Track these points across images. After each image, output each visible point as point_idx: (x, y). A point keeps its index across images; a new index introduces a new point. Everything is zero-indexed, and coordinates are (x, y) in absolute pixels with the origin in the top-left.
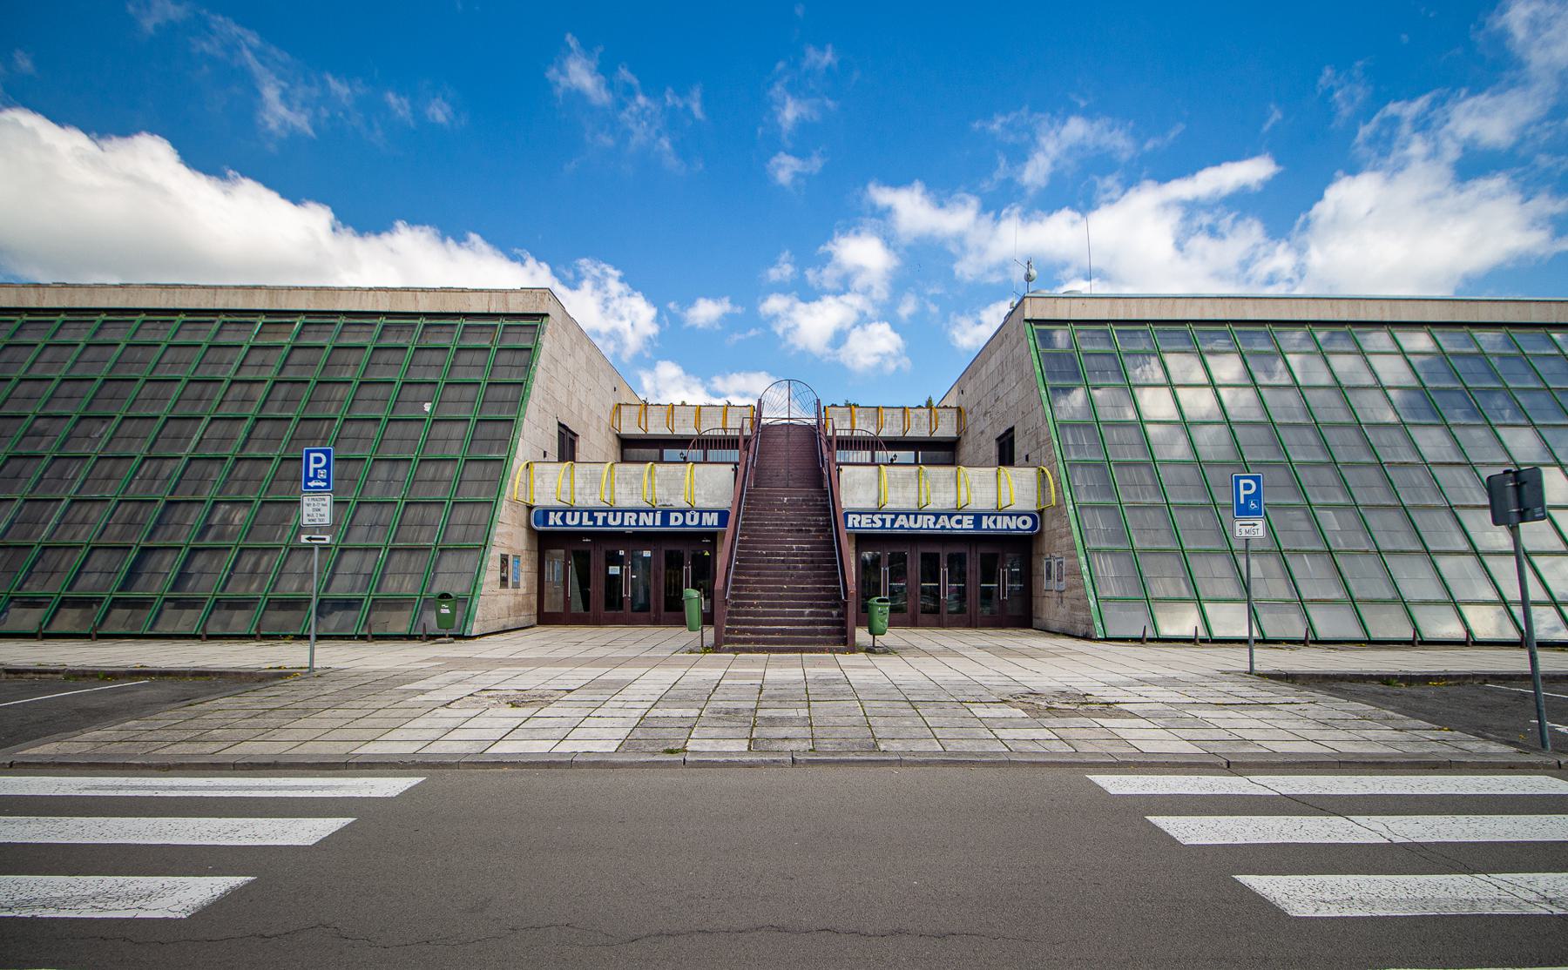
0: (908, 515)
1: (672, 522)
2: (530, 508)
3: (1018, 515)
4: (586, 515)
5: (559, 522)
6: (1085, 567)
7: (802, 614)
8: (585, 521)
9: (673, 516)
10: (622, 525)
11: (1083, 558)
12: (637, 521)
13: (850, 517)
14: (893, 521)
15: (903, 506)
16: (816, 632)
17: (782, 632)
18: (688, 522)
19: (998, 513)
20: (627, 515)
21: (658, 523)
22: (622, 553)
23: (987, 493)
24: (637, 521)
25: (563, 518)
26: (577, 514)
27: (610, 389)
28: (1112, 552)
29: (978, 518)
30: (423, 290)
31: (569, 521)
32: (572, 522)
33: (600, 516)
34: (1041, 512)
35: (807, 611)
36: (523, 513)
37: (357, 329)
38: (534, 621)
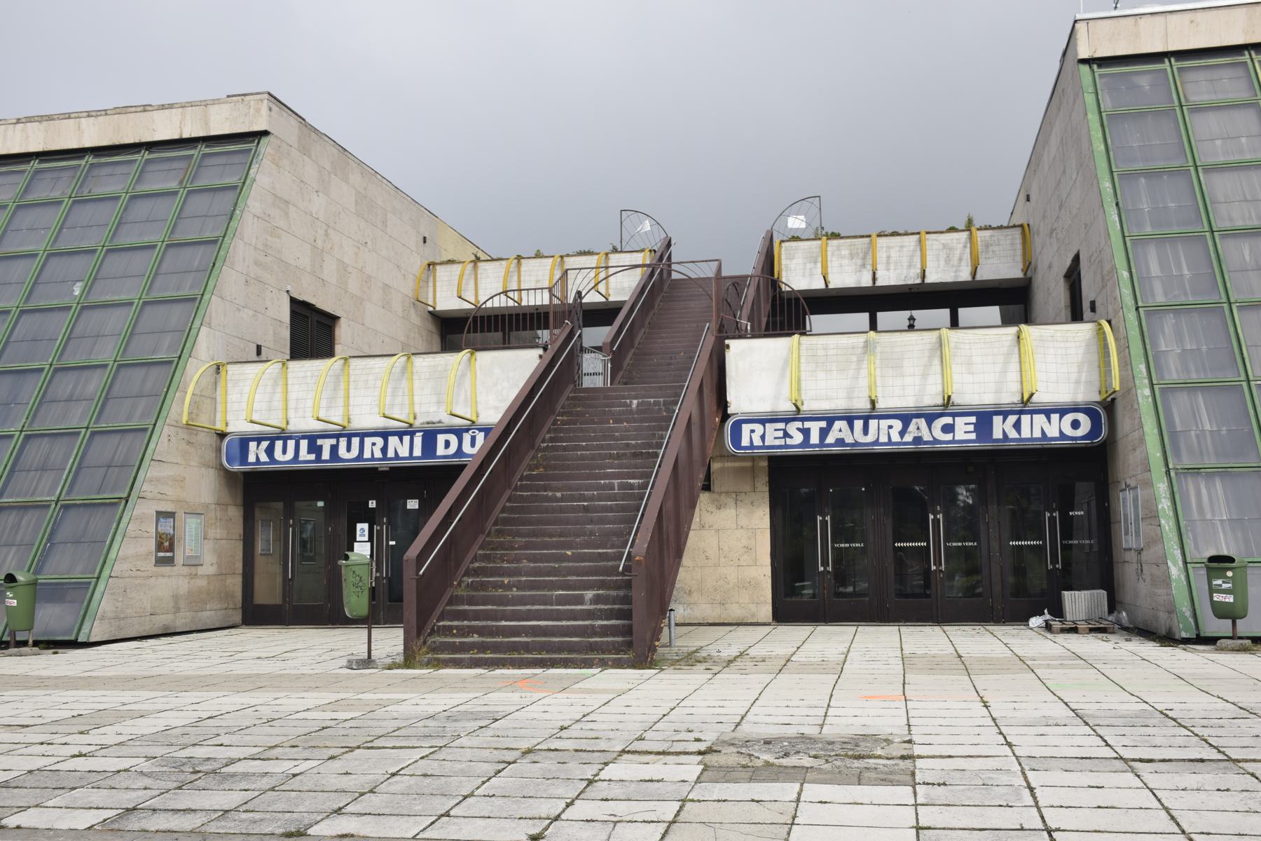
0: (850, 420)
1: (441, 450)
2: (222, 435)
3: (1063, 411)
4: (304, 444)
5: (264, 458)
6: (1165, 504)
9: (441, 439)
11: (1162, 487)
12: (384, 450)
13: (746, 428)
14: (824, 433)
15: (837, 403)
18: (467, 448)
19: (1025, 407)
21: (417, 452)
22: (372, 504)
23: (1032, 376)
24: (384, 450)
25: (270, 451)
27: (413, 240)
28: (1224, 473)
29: (984, 419)
30: (89, 114)
31: (278, 454)
32: (284, 456)
33: (326, 444)
35: (589, 594)
36: (208, 440)
37: (166, 166)
38: (238, 618)
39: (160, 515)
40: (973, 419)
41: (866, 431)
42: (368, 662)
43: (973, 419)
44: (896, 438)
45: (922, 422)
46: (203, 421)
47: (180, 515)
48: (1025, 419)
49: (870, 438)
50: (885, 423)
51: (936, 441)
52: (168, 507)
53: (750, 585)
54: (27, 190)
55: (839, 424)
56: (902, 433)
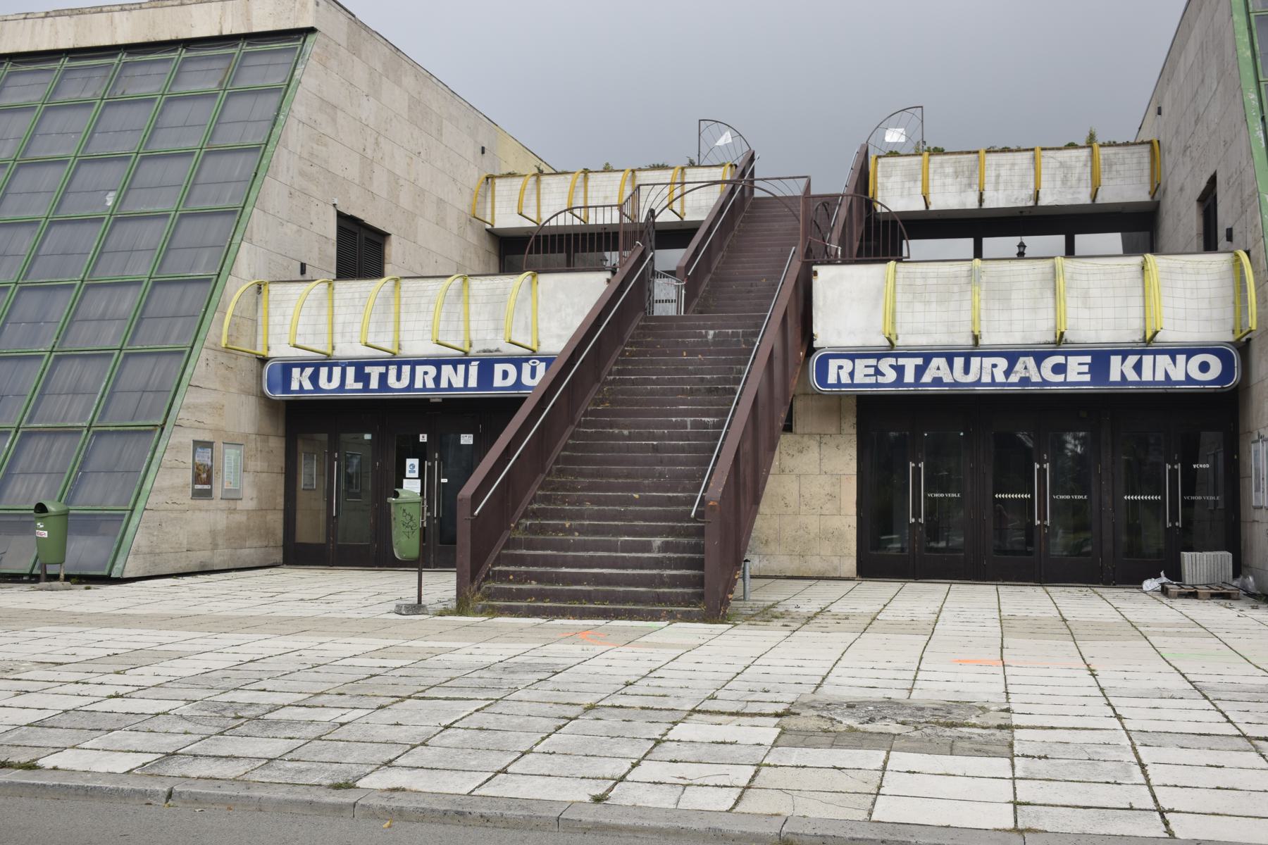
0: (950, 357)
1: (498, 381)
2: (263, 360)
3: (1190, 352)
4: (351, 371)
5: (308, 385)
7: (647, 547)
8: (351, 383)
9: (499, 369)
10: (411, 387)
12: (437, 379)
13: (833, 364)
14: (920, 371)
16: (661, 581)
17: (598, 579)
18: (527, 380)
19: (1148, 346)
20: (420, 370)
21: (473, 383)
22: (423, 438)
24: (437, 379)
25: (314, 378)
26: (337, 371)
27: (471, 151)
29: (1100, 359)
31: (323, 383)
32: (329, 384)
33: (375, 372)
34: (1244, 346)
35: (658, 541)
36: (248, 365)
38: (279, 557)
39: (198, 444)
40: (1088, 359)
41: (967, 370)
42: (417, 608)
43: (1088, 359)
44: (1000, 378)
45: (1030, 361)
46: (243, 344)
47: (218, 445)
48: (1148, 360)
49: (971, 378)
50: (988, 361)
51: (1045, 382)
52: (206, 437)
53: (836, 536)
54: (55, 91)
55: (935, 362)
56: (1008, 373)
